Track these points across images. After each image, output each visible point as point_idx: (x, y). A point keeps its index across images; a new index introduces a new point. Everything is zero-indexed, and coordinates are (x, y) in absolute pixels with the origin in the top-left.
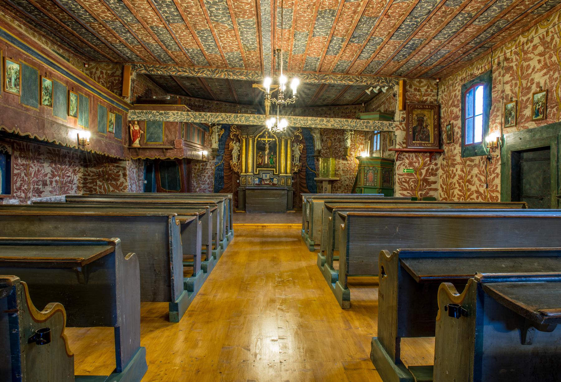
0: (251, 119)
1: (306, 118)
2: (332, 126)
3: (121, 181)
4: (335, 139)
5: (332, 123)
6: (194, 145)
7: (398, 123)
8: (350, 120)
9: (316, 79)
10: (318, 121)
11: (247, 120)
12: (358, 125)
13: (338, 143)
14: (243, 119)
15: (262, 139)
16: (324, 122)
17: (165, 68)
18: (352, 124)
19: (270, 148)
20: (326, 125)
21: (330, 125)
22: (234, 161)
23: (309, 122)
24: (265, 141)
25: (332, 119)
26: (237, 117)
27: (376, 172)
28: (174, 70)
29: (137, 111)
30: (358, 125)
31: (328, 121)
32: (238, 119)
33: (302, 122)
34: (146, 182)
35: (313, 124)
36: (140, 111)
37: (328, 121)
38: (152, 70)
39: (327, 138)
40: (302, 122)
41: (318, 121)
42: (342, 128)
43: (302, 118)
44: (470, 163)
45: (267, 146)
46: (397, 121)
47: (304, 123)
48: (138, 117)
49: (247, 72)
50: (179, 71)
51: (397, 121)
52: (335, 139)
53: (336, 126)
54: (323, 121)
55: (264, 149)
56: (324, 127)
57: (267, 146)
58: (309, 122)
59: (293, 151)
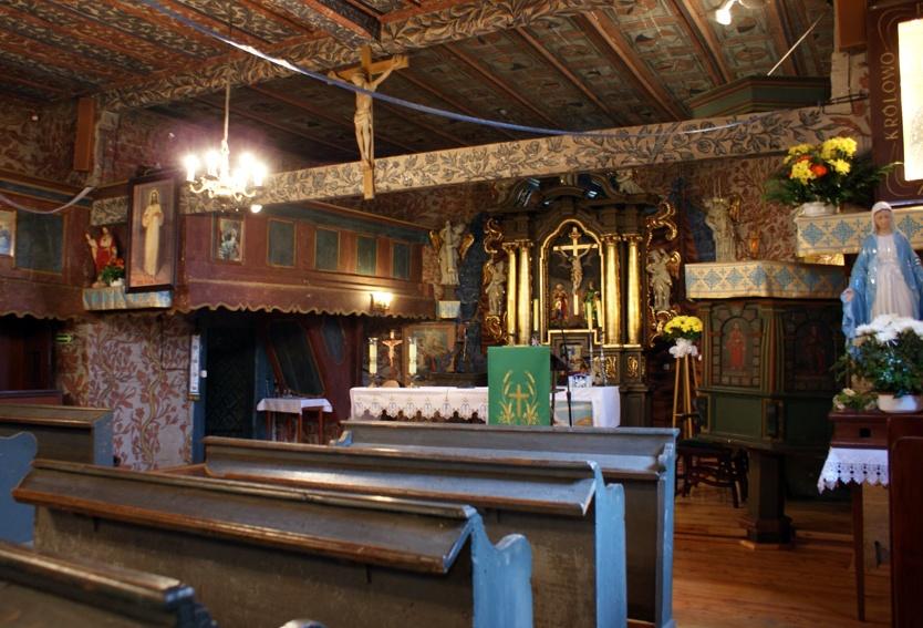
0: (330, 179)
1: (480, 148)
2: (569, 161)
3: (78, 372)
4: (772, 230)
5: (569, 152)
6: (340, 278)
7: (847, 107)
8: (634, 131)
9: (507, 11)
10: (520, 154)
11: (318, 185)
12: (669, 146)
13: (780, 242)
14: (310, 182)
15: (564, 248)
16: (543, 154)
17: (152, 85)
18: (642, 143)
19: (585, 271)
20: (547, 164)
21: (563, 160)
22: (492, 314)
23: (493, 162)
24: (570, 253)
25: (568, 139)
26: (295, 179)
27: (756, 325)
28: (168, 84)
29: (106, 201)
30: (669, 146)
31: (554, 149)
32: (298, 185)
33: (469, 165)
34: (204, 374)
35: (504, 167)
36: (111, 200)
37: (554, 149)
38: (132, 98)
39: (752, 228)
40: (469, 165)
41: (520, 154)
42: (609, 165)
43: (468, 151)
44: (747, 140)
45: (576, 265)
46: (840, 101)
47: (477, 168)
48: (108, 215)
49: (315, 46)
50: (177, 86)
51: (840, 101)
52: (772, 230)
53: (584, 160)
54: (538, 148)
55: (566, 276)
56: (542, 170)
57: (576, 265)
58: (493, 162)
59: (644, 275)
